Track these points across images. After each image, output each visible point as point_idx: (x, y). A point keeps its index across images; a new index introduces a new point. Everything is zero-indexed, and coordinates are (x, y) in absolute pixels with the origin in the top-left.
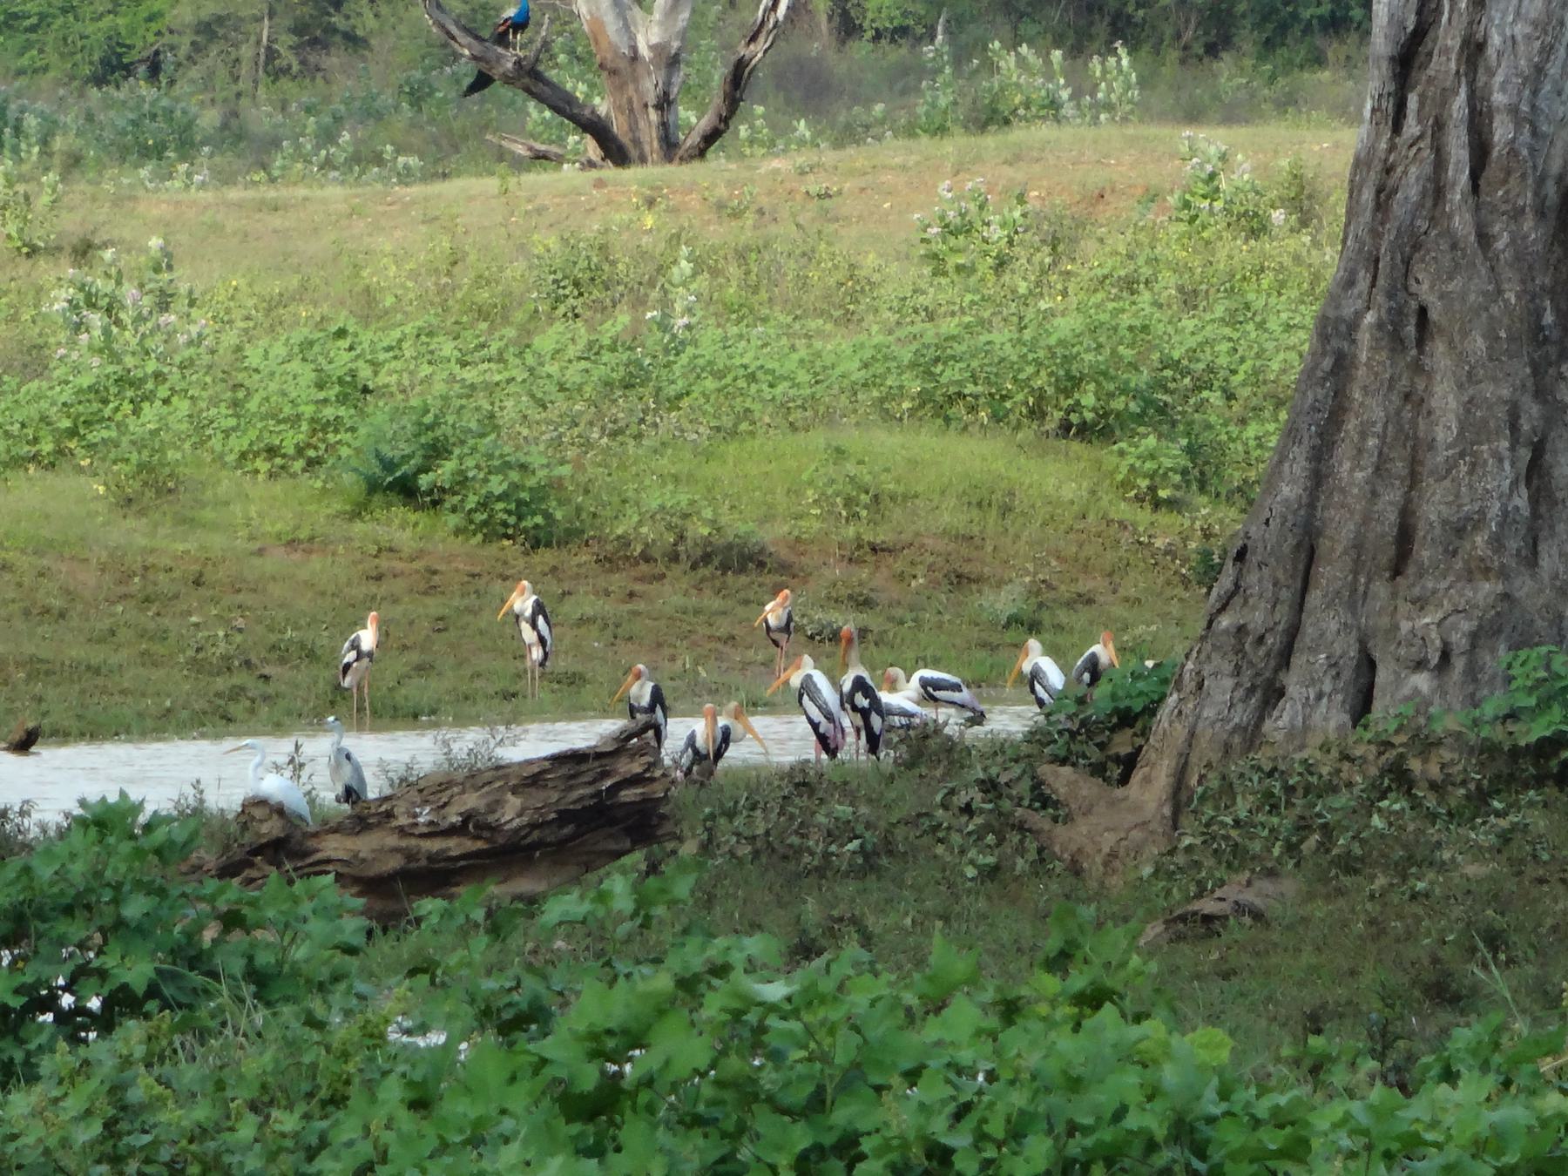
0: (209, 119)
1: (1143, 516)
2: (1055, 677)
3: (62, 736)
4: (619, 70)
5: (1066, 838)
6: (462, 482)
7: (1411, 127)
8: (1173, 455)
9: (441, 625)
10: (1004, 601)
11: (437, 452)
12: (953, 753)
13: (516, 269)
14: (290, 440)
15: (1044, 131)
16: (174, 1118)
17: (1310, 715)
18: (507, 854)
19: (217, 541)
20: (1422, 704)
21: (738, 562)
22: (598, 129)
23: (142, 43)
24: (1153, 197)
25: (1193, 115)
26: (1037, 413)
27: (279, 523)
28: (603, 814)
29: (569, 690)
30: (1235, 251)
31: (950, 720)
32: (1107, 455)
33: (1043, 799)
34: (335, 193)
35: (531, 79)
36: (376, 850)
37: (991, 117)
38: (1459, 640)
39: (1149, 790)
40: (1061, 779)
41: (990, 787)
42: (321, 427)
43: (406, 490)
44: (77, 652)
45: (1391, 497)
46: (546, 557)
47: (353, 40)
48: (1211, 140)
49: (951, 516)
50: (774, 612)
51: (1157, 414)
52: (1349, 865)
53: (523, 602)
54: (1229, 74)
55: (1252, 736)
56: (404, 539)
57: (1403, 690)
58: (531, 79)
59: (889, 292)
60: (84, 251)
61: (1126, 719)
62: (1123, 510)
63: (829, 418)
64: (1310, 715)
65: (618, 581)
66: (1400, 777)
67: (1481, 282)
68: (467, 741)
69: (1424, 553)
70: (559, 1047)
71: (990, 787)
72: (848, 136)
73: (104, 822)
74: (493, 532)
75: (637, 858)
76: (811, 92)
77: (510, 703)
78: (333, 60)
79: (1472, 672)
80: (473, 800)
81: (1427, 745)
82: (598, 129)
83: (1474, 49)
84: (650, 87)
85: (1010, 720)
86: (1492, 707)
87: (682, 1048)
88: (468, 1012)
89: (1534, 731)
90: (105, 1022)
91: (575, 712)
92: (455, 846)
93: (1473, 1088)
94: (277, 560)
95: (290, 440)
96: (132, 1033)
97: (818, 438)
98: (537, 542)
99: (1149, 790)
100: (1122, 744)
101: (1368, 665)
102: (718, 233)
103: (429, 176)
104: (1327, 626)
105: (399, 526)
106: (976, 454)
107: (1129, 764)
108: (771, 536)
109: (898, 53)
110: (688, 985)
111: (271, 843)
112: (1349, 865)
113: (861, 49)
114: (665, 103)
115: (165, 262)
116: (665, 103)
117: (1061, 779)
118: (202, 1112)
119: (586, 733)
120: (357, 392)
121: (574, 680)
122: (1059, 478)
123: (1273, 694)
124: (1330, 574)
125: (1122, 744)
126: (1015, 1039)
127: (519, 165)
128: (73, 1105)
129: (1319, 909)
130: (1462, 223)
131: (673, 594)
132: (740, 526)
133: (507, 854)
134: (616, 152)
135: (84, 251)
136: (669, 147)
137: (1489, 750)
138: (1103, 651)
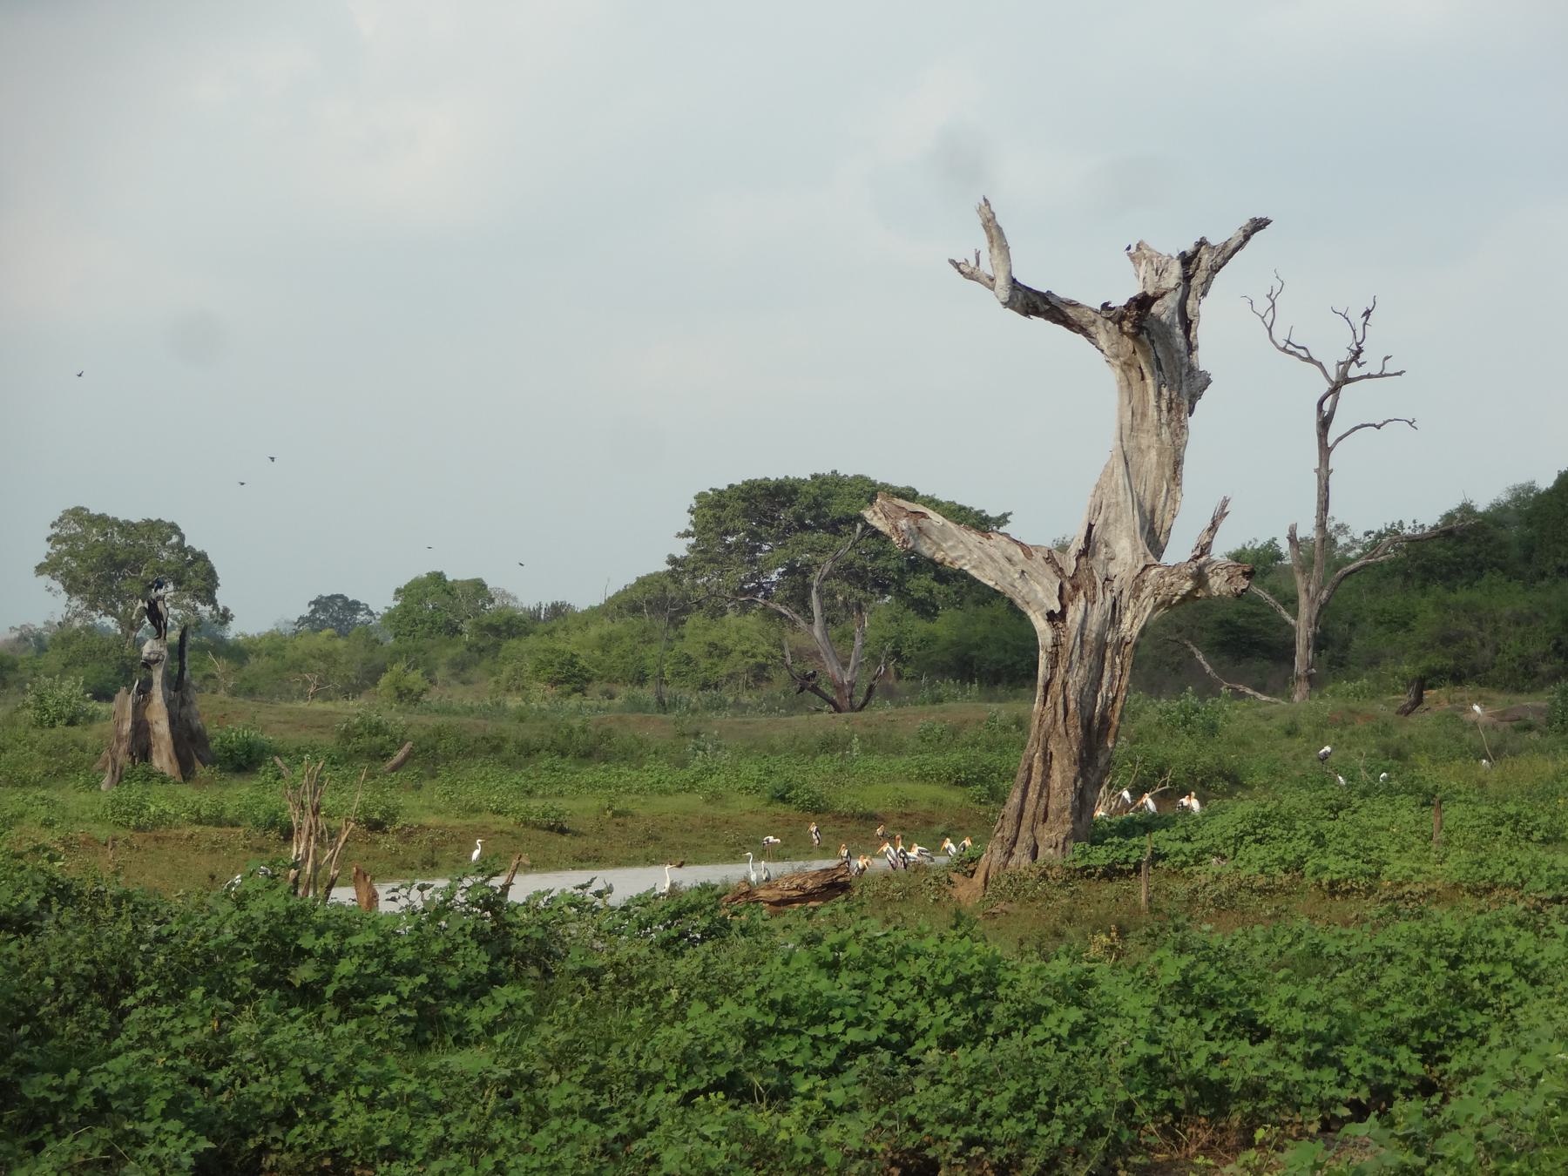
0: (731, 700)
1: (977, 806)
2: (954, 849)
3: (690, 863)
4: (839, 688)
5: (955, 893)
6: (797, 796)
7: (1048, 704)
8: (985, 790)
9: (791, 834)
10: (940, 829)
11: (790, 788)
12: (927, 870)
13: (812, 740)
14: (752, 785)
15: (951, 704)
16: (720, 967)
17: (1021, 858)
18: (808, 896)
19: (732, 812)
20: (1050, 856)
21: (870, 818)
22: (832, 702)
23: (713, 679)
24: (980, 722)
25: (990, 701)
26: (949, 779)
27: (749, 807)
28: (834, 887)
29: (825, 851)
30: (1001, 736)
31: (926, 862)
32: (968, 790)
33: (950, 882)
34: (764, 720)
35: (815, 689)
36: (774, 895)
37: (938, 700)
38: (1061, 840)
39: (979, 879)
40: (955, 877)
41: (936, 878)
42: (759, 781)
43: (782, 799)
44: (694, 841)
45: (1043, 801)
46: (819, 816)
47: (768, 679)
48: (995, 706)
49: (926, 806)
50: (879, 831)
51: (981, 780)
52: (1033, 900)
53: (814, 829)
54: (1000, 690)
55: (1005, 865)
56: (782, 812)
57: (1045, 853)
58: (815, 689)
59: (910, 747)
60: (697, 735)
61: (972, 860)
62: (972, 805)
63: (894, 780)
64: (1021, 858)
65: (838, 823)
66: (1044, 875)
67: (1067, 745)
68: (798, 864)
69: (1051, 817)
70: (823, 949)
71: (936, 878)
72: (899, 705)
73: (705, 888)
74: (805, 810)
75: (842, 897)
76: (890, 693)
77: (809, 854)
78: (764, 684)
79: (1064, 848)
80: (799, 881)
81: (1050, 868)
82: (832, 702)
83: (1065, 685)
84: (847, 692)
85: (941, 860)
86: (1070, 857)
87: (854, 950)
88: (799, 939)
89: (1079, 865)
90: (702, 941)
91: (826, 858)
92: (795, 893)
93: (1064, 961)
94: (1085, 661)
95: (752, 785)
96: (709, 945)
97: (891, 785)
98: (817, 812)
99: (979, 879)
100: (971, 867)
101: (1036, 847)
102: (865, 731)
103: (788, 715)
104: (1025, 835)
105: (780, 808)
106: (932, 790)
107: (973, 872)
108: (879, 811)
109: (913, 683)
110: (857, 933)
111: (748, 894)
112: (1033, 900)
113: (903, 682)
114: (851, 696)
115: (720, 737)
116: (851, 696)
117: (955, 877)
118: (728, 965)
119: (830, 863)
120: (769, 773)
121: (826, 849)
122: (955, 797)
123: (1010, 854)
124: (1026, 822)
125: (971, 867)
126: (943, 946)
127: (812, 713)
128: (695, 962)
129: (1023, 911)
130: (1062, 730)
131: (852, 827)
132: (870, 808)
133: (808, 896)
134: (838, 709)
135: (697, 735)
136: (852, 709)
137: (1069, 869)
138: (967, 842)
